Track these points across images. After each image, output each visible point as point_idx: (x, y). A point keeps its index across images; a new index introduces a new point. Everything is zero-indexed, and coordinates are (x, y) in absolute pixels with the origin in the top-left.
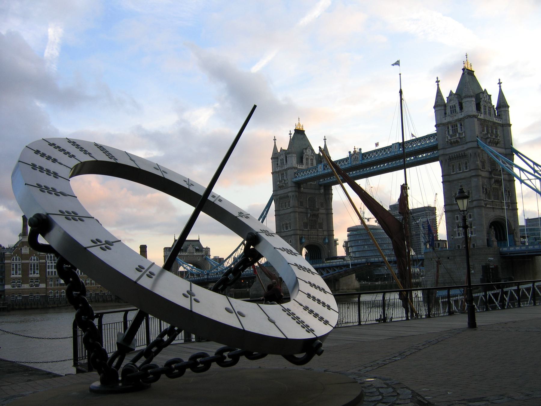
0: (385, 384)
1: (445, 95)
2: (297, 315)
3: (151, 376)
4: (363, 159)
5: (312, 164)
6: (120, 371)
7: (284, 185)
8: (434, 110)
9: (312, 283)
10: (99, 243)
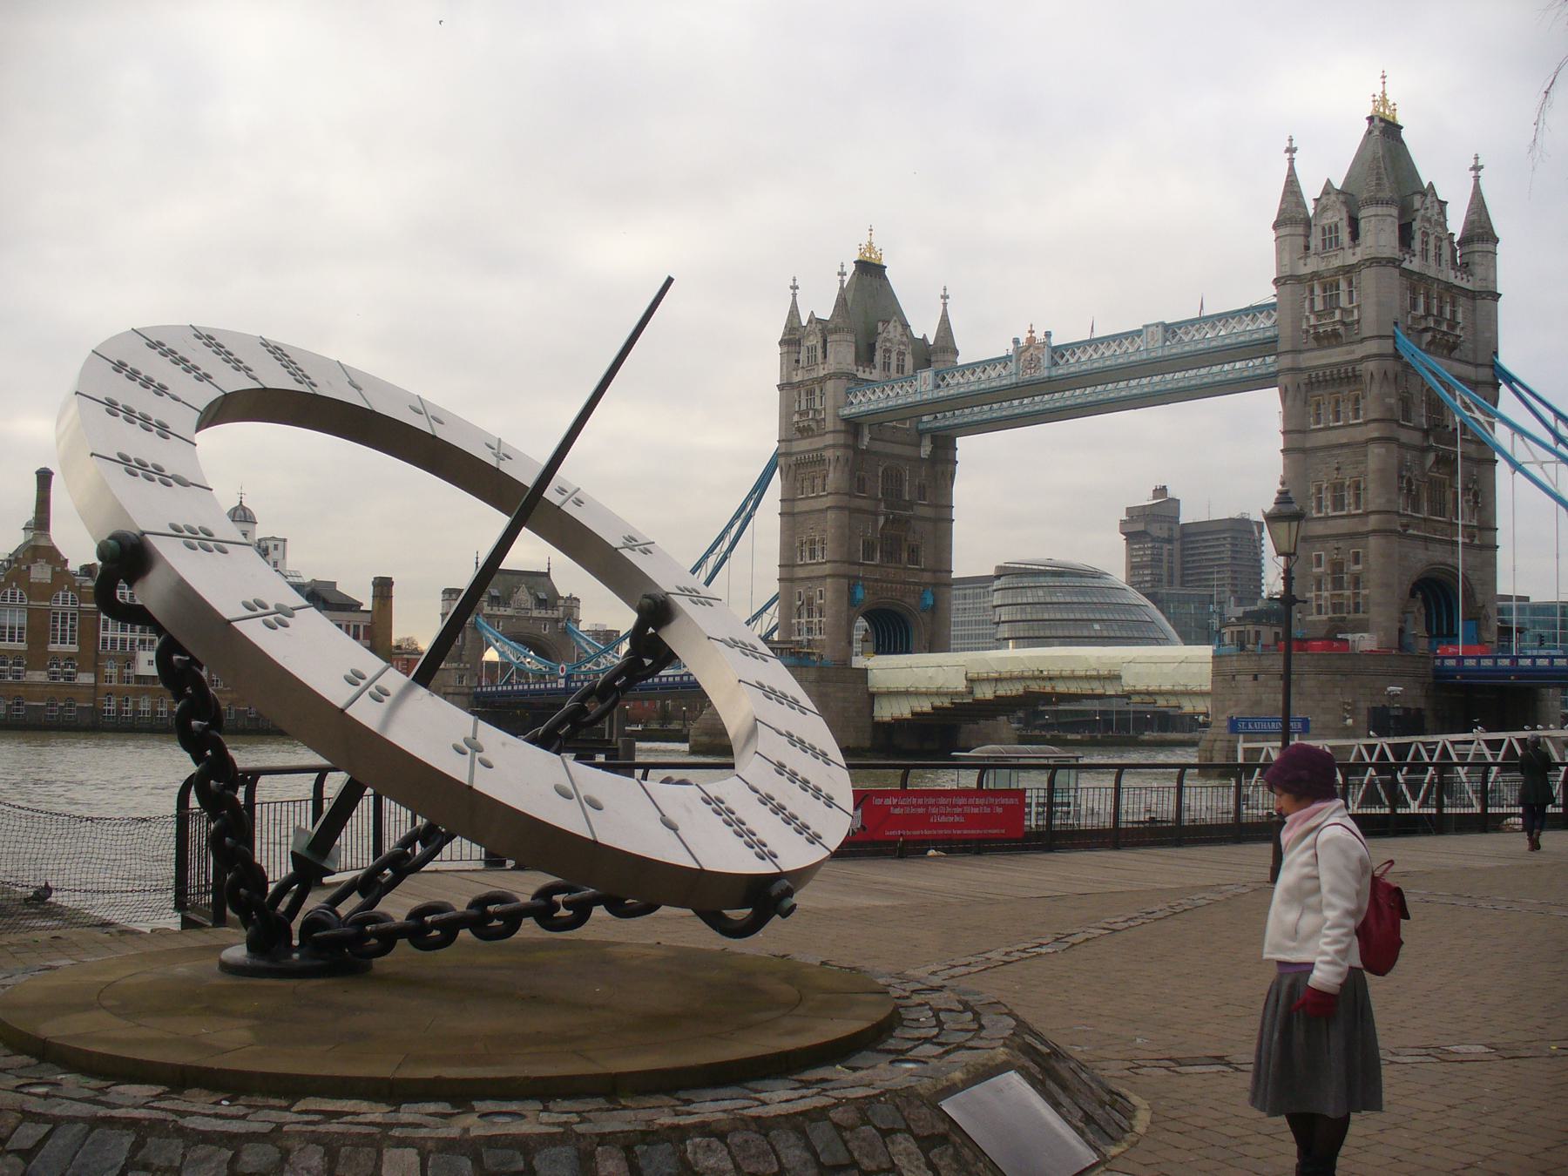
1: (1311, 192)
3: (373, 941)
6: (296, 926)
7: (814, 425)
8: (1273, 235)
10: (261, 611)
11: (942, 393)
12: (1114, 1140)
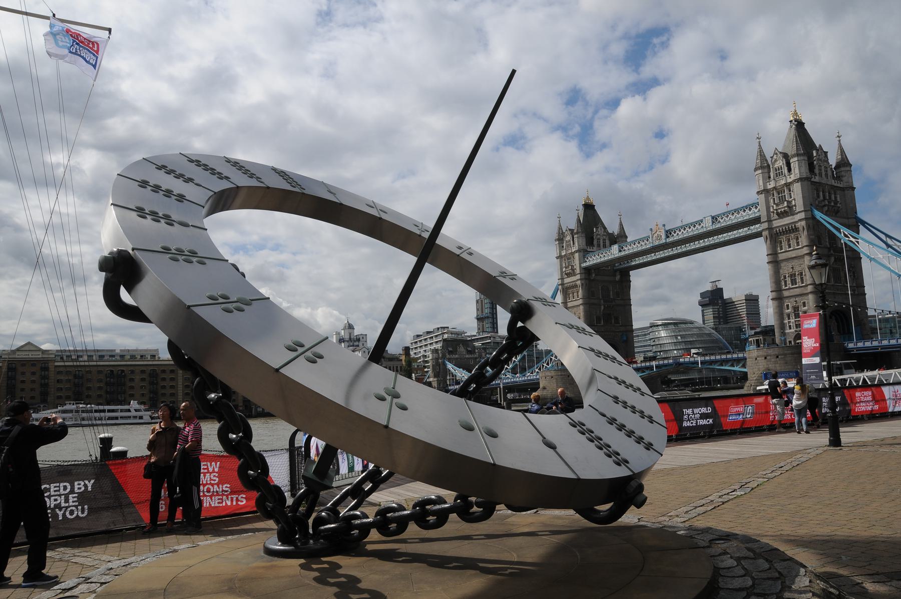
0: (749, 549)
1: (768, 154)
2: (615, 447)
4: (668, 237)
6: (311, 521)
9: (620, 378)
11: (623, 253)
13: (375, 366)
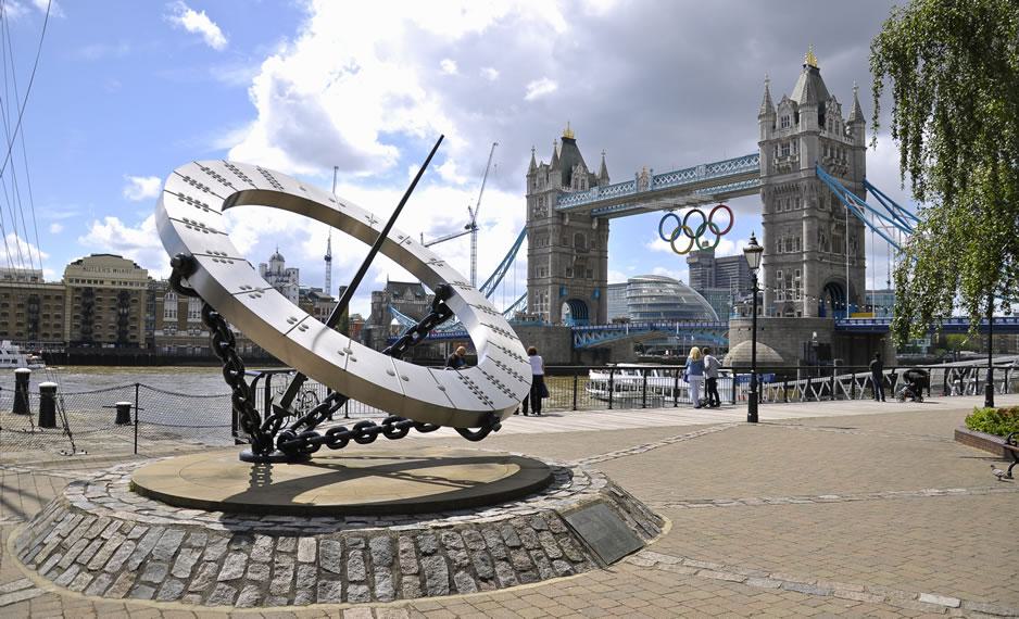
5: (583, 187)
6: (275, 440)
12: (652, 537)
13: (331, 331)
